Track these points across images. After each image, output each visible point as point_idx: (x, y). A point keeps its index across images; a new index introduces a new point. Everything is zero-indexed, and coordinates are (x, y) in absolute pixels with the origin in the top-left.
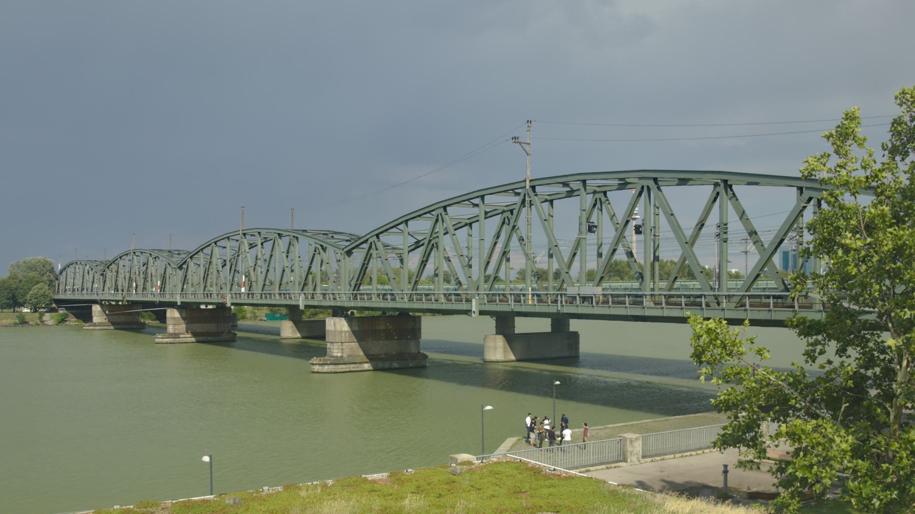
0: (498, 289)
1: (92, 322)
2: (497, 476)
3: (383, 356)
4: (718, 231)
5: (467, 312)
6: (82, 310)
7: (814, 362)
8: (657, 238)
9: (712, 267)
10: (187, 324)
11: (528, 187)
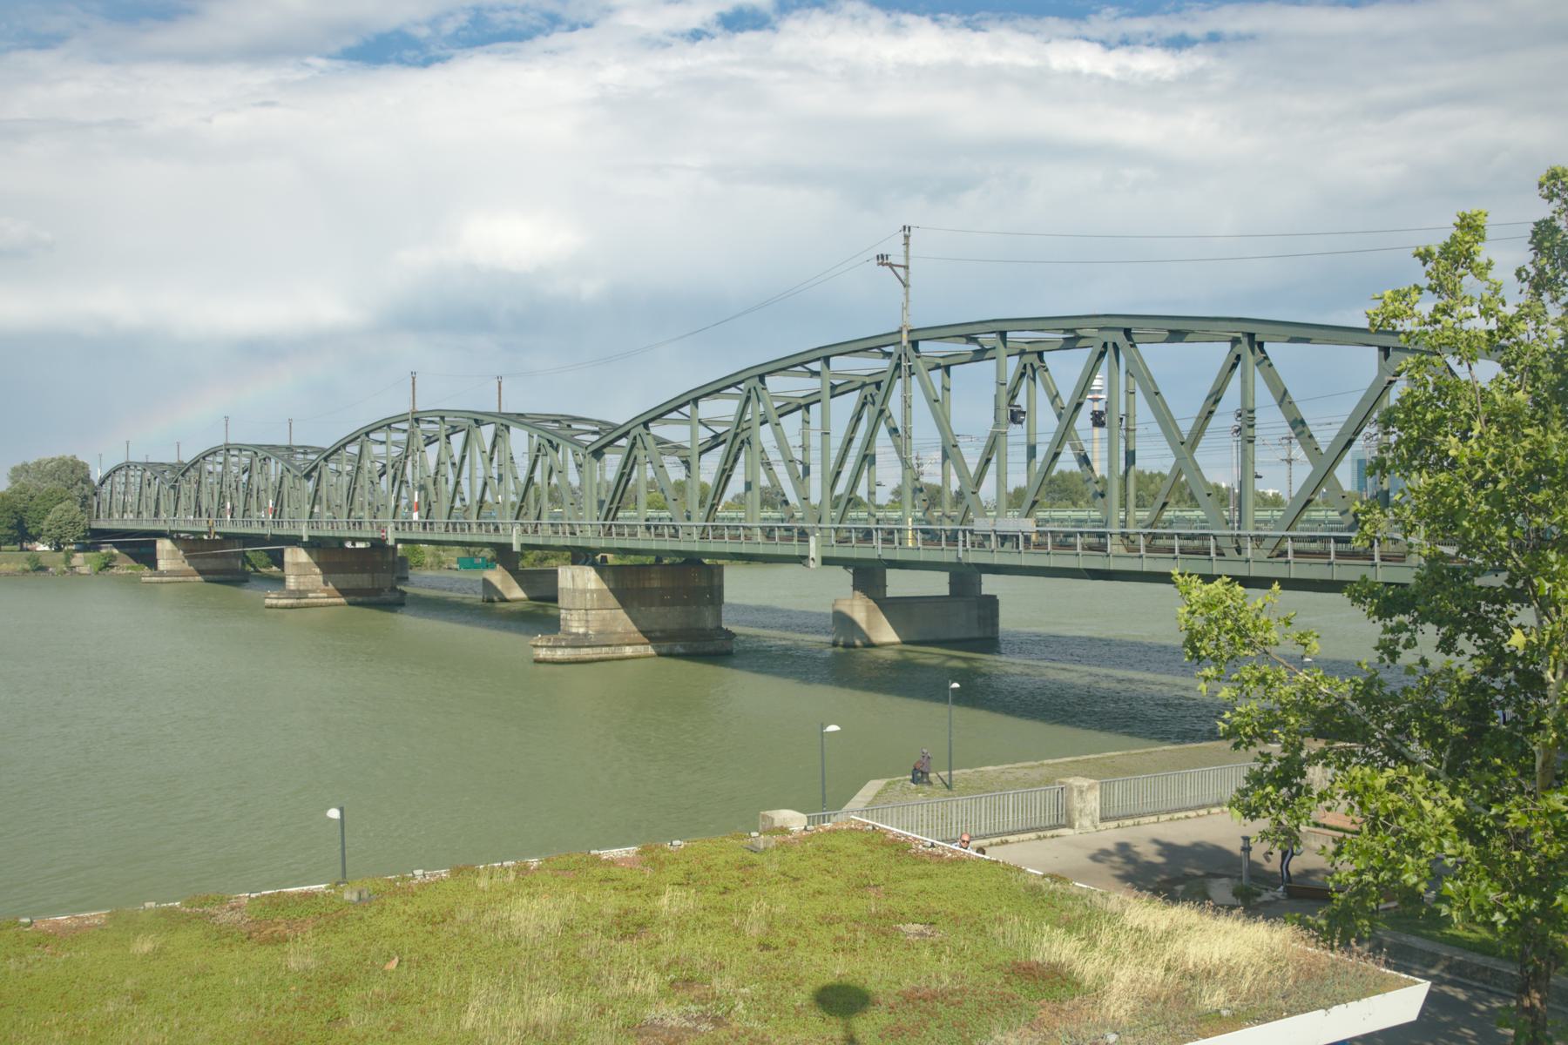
0: (854, 520)
1: (156, 569)
2: (829, 855)
3: (658, 634)
4: (1239, 423)
5: (802, 559)
6: (141, 548)
8: (1131, 434)
11: (905, 343)
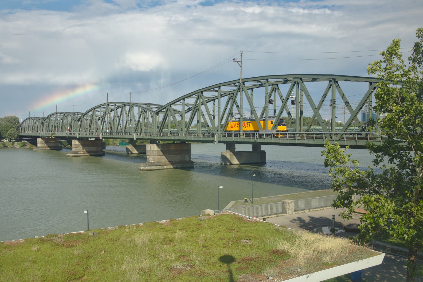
1: (37, 146)
2: (221, 221)
4: (331, 103)
5: (212, 142)
6: (33, 140)
7: (378, 165)
9: (328, 120)
11: (241, 82)
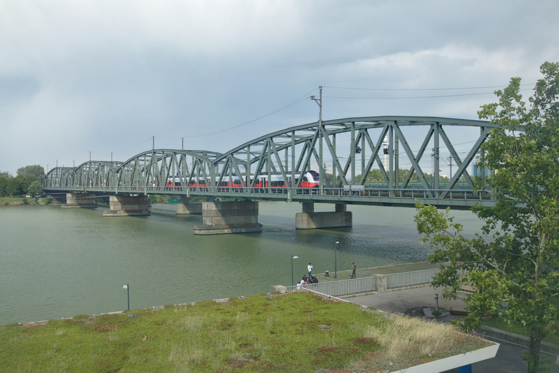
1: (66, 203)
2: (294, 301)
3: (236, 225)
7: (488, 233)
8: (397, 156)
10: (122, 205)
11: (320, 126)
